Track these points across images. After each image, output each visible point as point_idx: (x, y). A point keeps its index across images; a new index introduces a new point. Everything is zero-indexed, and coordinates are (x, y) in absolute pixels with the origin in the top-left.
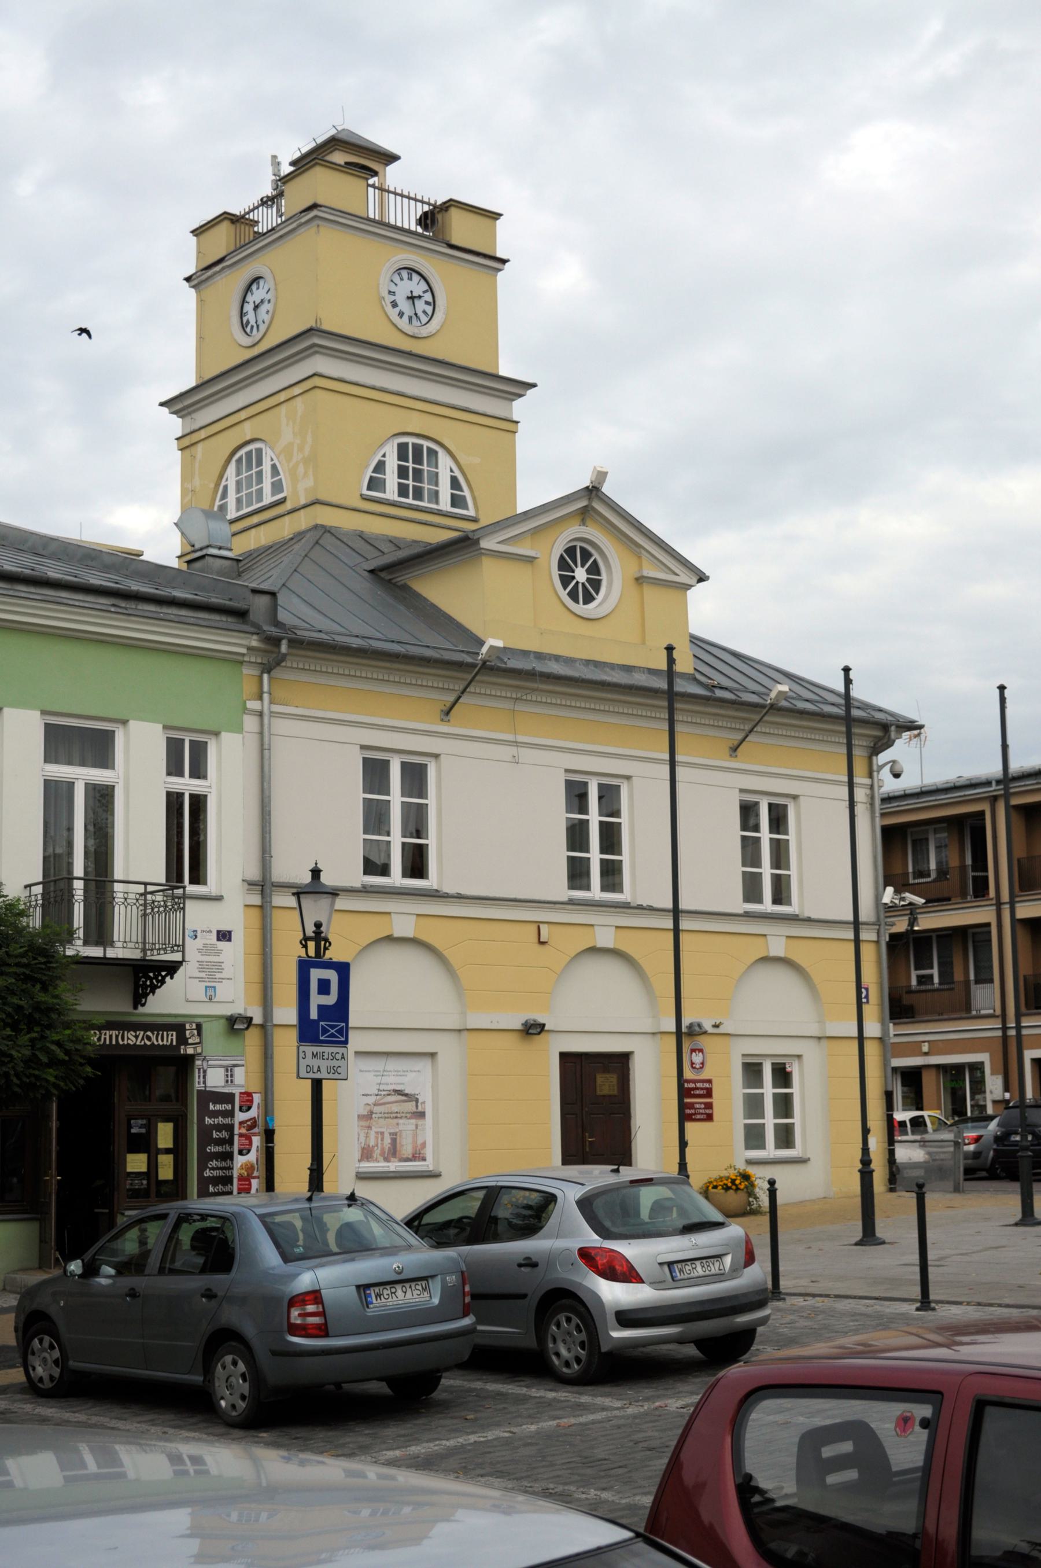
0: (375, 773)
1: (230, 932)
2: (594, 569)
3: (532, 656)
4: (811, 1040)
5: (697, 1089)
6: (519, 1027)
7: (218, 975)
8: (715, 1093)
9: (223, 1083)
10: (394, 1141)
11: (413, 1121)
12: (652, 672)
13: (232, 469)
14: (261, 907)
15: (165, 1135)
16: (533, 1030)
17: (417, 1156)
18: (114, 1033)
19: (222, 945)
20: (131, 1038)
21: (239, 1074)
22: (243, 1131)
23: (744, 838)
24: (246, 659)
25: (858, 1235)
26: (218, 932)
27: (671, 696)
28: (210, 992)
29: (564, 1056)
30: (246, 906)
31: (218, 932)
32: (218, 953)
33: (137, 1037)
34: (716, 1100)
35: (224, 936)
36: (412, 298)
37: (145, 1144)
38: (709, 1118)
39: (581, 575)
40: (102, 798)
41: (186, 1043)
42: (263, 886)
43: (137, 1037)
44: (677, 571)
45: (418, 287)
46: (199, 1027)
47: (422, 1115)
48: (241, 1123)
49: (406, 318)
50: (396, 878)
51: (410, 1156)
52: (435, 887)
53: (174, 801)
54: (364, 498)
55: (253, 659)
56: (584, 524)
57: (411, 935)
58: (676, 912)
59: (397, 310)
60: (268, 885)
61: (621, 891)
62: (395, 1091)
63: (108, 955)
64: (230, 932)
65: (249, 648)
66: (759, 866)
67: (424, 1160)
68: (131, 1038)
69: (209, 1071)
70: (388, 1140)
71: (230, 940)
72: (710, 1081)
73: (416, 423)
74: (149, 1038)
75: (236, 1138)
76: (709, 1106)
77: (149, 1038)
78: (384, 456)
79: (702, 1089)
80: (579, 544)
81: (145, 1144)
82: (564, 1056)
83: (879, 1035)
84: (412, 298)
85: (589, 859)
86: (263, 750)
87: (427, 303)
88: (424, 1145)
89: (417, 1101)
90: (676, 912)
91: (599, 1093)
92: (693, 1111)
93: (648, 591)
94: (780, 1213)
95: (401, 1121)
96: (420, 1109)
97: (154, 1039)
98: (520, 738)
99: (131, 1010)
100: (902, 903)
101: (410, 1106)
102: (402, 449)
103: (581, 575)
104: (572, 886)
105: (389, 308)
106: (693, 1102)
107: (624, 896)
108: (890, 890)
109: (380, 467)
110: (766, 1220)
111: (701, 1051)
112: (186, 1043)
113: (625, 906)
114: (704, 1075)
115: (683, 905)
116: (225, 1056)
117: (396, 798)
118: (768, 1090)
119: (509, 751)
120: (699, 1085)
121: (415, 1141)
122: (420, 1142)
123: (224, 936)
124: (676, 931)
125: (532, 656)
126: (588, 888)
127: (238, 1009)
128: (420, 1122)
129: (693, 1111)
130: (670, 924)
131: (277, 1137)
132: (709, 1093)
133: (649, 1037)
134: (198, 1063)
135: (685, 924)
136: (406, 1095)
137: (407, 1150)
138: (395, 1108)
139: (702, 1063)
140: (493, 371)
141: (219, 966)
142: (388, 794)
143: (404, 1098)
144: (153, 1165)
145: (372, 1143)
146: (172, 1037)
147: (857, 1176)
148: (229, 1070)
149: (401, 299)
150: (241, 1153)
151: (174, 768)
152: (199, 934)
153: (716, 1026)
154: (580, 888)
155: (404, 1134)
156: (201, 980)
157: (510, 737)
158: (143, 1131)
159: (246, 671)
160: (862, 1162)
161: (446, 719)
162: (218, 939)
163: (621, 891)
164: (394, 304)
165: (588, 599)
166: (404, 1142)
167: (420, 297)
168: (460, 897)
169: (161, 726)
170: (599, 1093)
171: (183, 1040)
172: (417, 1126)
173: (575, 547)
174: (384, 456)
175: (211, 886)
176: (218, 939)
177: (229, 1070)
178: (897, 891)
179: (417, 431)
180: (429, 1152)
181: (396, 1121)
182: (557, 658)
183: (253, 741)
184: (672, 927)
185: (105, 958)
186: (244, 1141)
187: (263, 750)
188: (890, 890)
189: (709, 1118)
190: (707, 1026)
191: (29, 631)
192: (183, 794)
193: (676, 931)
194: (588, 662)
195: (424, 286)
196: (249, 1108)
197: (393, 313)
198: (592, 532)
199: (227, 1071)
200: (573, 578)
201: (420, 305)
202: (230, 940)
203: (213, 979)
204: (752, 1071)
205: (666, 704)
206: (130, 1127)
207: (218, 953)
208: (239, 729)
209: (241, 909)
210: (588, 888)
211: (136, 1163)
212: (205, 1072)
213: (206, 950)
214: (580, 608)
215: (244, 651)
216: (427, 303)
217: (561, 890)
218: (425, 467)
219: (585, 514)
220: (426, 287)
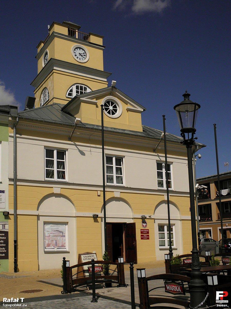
0: (49, 152)
1: (4, 191)
2: (115, 107)
5: (145, 232)
10: (56, 243)
13: (42, 95)
17: (63, 246)
21: (7, 227)
30: (9, 185)
34: (150, 234)
38: (148, 239)
39: (111, 108)
44: (138, 107)
50: (55, 178)
51: (61, 246)
54: (67, 97)
59: (76, 57)
60: (15, 180)
62: (56, 230)
64: (4, 191)
70: (54, 242)
71: (4, 193)
72: (148, 230)
73: (80, 81)
76: (148, 236)
78: (72, 88)
79: (146, 232)
88: (65, 243)
89: (63, 233)
92: (143, 237)
96: (63, 235)
100: (201, 188)
101: (61, 234)
102: (77, 87)
103: (111, 108)
108: (198, 185)
109: (71, 91)
110: (129, 288)
116: (3, 222)
121: (62, 242)
126: (113, 183)
127: (7, 210)
128: (64, 238)
129: (143, 237)
132: (148, 233)
137: (60, 245)
138: (56, 234)
139: (146, 225)
143: (59, 232)
145: (50, 243)
149: (78, 55)
153: (150, 217)
164: (76, 55)
165: (113, 114)
174: (72, 88)
178: (200, 185)
181: (57, 238)
183: (12, 144)
184: (103, 190)
188: (198, 185)
189: (148, 239)
190: (148, 217)
195: (83, 52)
197: (75, 58)
199: (3, 225)
202: (4, 193)
208: (7, 141)
210: (113, 183)
214: (111, 116)
218: (83, 91)
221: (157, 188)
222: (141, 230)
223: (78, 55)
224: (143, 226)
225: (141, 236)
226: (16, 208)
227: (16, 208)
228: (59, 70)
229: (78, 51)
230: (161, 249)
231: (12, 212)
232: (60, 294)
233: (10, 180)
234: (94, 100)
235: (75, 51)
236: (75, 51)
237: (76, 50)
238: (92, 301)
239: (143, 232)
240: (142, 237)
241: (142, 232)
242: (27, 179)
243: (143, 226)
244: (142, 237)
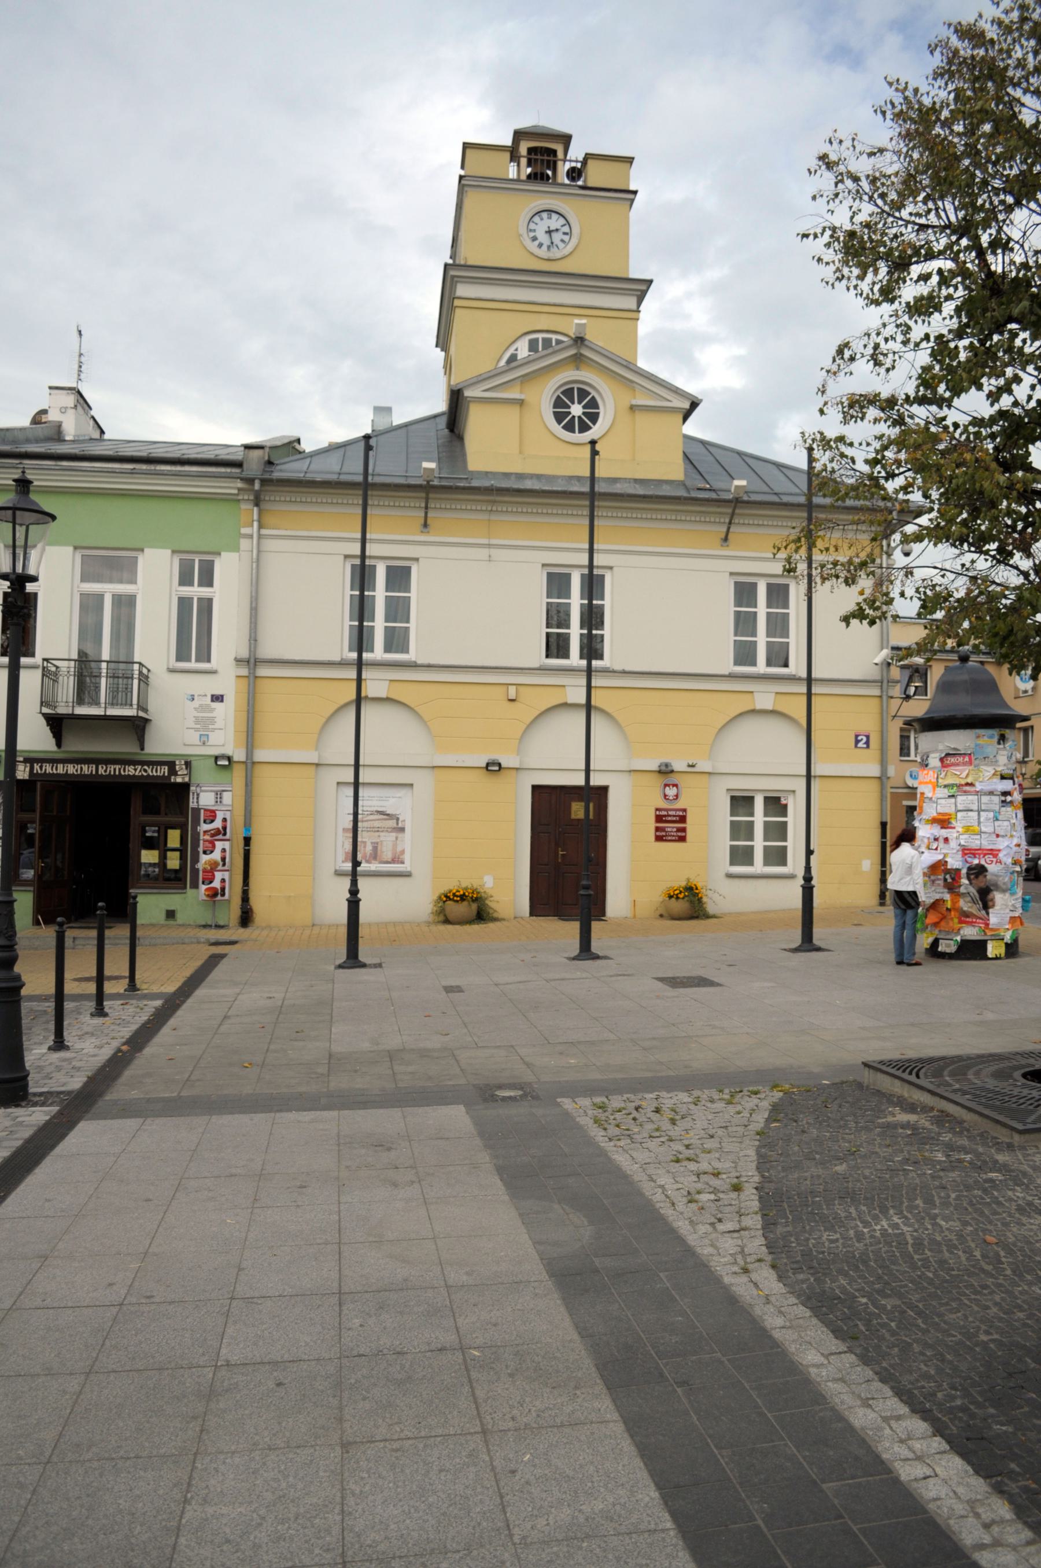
1: (222, 696)
3: (513, 478)
4: (649, 775)
6: (655, 768)
7: (211, 727)
8: (688, 820)
9: (213, 803)
11: (394, 834)
12: (579, 478)
14: (881, 697)
15: (174, 838)
16: (493, 767)
17: (397, 859)
18: (117, 767)
19: (216, 705)
20: (130, 770)
21: (227, 798)
22: (207, 837)
23: (738, 614)
24: (240, 497)
25: (576, 951)
26: (212, 696)
27: (592, 496)
28: (204, 739)
29: (535, 788)
30: (238, 677)
31: (212, 696)
32: (212, 710)
33: (135, 770)
34: (689, 825)
35: (218, 698)
36: (549, 232)
37: (157, 844)
39: (577, 410)
40: (126, 605)
41: (176, 774)
42: (251, 663)
43: (135, 770)
45: (555, 222)
46: (188, 764)
47: (402, 830)
48: (205, 832)
49: (545, 247)
50: (761, 667)
52: (413, 659)
53: (184, 603)
55: (246, 497)
56: (578, 369)
57: (384, 696)
58: (809, 680)
59: (536, 243)
61: (407, 652)
62: (378, 812)
63: (108, 713)
64: (222, 696)
65: (239, 489)
66: (754, 634)
67: (403, 863)
68: (130, 770)
69: (202, 795)
71: (222, 701)
72: (685, 810)
73: (544, 322)
74: (145, 771)
75: (201, 842)
76: (684, 830)
77: (145, 771)
80: (576, 386)
81: (157, 844)
82: (535, 788)
83: (878, 775)
84: (549, 232)
85: (756, 642)
86: (258, 562)
87: (565, 234)
88: (403, 852)
89: (398, 819)
90: (809, 680)
91: (573, 816)
93: (641, 418)
94: (362, 931)
95: (382, 834)
96: (400, 825)
97: (149, 771)
98: (494, 541)
99: (138, 751)
101: (392, 823)
103: (577, 410)
104: (738, 662)
105: (528, 243)
106: (671, 826)
107: (411, 656)
111: (676, 785)
112: (176, 774)
113: (413, 666)
114: (680, 804)
115: (815, 675)
117: (762, 609)
118: (759, 817)
119: (484, 553)
120: (670, 813)
122: (399, 849)
123: (218, 698)
124: (809, 695)
125: (513, 478)
128: (400, 835)
130: (804, 690)
131: (253, 843)
132: (683, 819)
133: (627, 774)
134: (192, 788)
135: (815, 690)
136: (388, 815)
137: (388, 856)
138: (377, 824)
139: (677, 796)
140: (624, 276)
141: (212, 721)
142: (756, 607)
144: (163, 857)
146: (165, 770)
147: (345, 906)
148: (219, 795)
150: (205, 852)
151: (185, 579)
152: (196, 698)
154: (563, 657)
155: (385, 843)
156: (197, 730)
157: (485, 541)
158: (156, 835)
159: (244, 506)
160: (804, 878)
161: (425, 530)
162: (212, 701)
163: (407, 652)
164: (534, 239)
166: (384, 849)
167: (557, 230)
168: (429, 666)
169: (169, 552)
170: (573, 816)
171: (173, 771)
172: (397, 838)
173: (573, 389)
175: (213, 664)
176: (212, 701)
177: (219, 795)
179: (545, 328)
180: (407, 857)
181: (377, 834)
182: (532, 476)
185: (73, 714)
186: (207, 844)
187: (258, 562)
189: (682, 839)
191: (197, 498)
192: (193, 598)
193: (809, 695)
194: (571, 478)
195: (562, 221)
196: (212, 821)
198: (585, 375)
200: (574, 417)
201: (557, 237)
202: (222, 701)
203: (208, 730)
204: (741, 802)
205: (587, 503)
206: (144, 831)
207: (212, 710)
208: (236, 549)
209: (233, 679)
211: (149, 857)
212: (198, 795)
213: (202, 708)
215: (236, 492)
216: (565, 234)
217: (728, 666)
219: (578, 360)
220: (564, 222)
221: (728, 666)
222: (657, 810)
223: (543, 238)
224: (665, 796)
225: (657, 829)
226: (250, 745)
227: (250, 745)
228: (473, 296)
229: (542, 225)
230: (730, 876)
231: (239, 755)
232: (122, 991)
233: (238, 661)
234: (514, 394)
235: (532, 226)
236: (532, 226)
237: (536, 219)
238: (92, 1015)
239: (665, 816)
240: (658, 834)
241: (659, 819)
242: (297, 658)
243: (665, 796)
244: (658, 834)
